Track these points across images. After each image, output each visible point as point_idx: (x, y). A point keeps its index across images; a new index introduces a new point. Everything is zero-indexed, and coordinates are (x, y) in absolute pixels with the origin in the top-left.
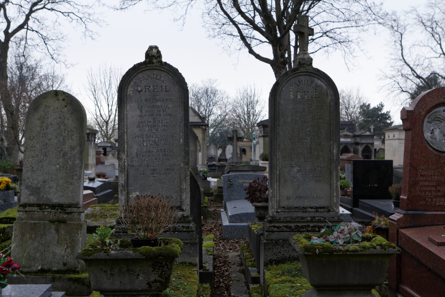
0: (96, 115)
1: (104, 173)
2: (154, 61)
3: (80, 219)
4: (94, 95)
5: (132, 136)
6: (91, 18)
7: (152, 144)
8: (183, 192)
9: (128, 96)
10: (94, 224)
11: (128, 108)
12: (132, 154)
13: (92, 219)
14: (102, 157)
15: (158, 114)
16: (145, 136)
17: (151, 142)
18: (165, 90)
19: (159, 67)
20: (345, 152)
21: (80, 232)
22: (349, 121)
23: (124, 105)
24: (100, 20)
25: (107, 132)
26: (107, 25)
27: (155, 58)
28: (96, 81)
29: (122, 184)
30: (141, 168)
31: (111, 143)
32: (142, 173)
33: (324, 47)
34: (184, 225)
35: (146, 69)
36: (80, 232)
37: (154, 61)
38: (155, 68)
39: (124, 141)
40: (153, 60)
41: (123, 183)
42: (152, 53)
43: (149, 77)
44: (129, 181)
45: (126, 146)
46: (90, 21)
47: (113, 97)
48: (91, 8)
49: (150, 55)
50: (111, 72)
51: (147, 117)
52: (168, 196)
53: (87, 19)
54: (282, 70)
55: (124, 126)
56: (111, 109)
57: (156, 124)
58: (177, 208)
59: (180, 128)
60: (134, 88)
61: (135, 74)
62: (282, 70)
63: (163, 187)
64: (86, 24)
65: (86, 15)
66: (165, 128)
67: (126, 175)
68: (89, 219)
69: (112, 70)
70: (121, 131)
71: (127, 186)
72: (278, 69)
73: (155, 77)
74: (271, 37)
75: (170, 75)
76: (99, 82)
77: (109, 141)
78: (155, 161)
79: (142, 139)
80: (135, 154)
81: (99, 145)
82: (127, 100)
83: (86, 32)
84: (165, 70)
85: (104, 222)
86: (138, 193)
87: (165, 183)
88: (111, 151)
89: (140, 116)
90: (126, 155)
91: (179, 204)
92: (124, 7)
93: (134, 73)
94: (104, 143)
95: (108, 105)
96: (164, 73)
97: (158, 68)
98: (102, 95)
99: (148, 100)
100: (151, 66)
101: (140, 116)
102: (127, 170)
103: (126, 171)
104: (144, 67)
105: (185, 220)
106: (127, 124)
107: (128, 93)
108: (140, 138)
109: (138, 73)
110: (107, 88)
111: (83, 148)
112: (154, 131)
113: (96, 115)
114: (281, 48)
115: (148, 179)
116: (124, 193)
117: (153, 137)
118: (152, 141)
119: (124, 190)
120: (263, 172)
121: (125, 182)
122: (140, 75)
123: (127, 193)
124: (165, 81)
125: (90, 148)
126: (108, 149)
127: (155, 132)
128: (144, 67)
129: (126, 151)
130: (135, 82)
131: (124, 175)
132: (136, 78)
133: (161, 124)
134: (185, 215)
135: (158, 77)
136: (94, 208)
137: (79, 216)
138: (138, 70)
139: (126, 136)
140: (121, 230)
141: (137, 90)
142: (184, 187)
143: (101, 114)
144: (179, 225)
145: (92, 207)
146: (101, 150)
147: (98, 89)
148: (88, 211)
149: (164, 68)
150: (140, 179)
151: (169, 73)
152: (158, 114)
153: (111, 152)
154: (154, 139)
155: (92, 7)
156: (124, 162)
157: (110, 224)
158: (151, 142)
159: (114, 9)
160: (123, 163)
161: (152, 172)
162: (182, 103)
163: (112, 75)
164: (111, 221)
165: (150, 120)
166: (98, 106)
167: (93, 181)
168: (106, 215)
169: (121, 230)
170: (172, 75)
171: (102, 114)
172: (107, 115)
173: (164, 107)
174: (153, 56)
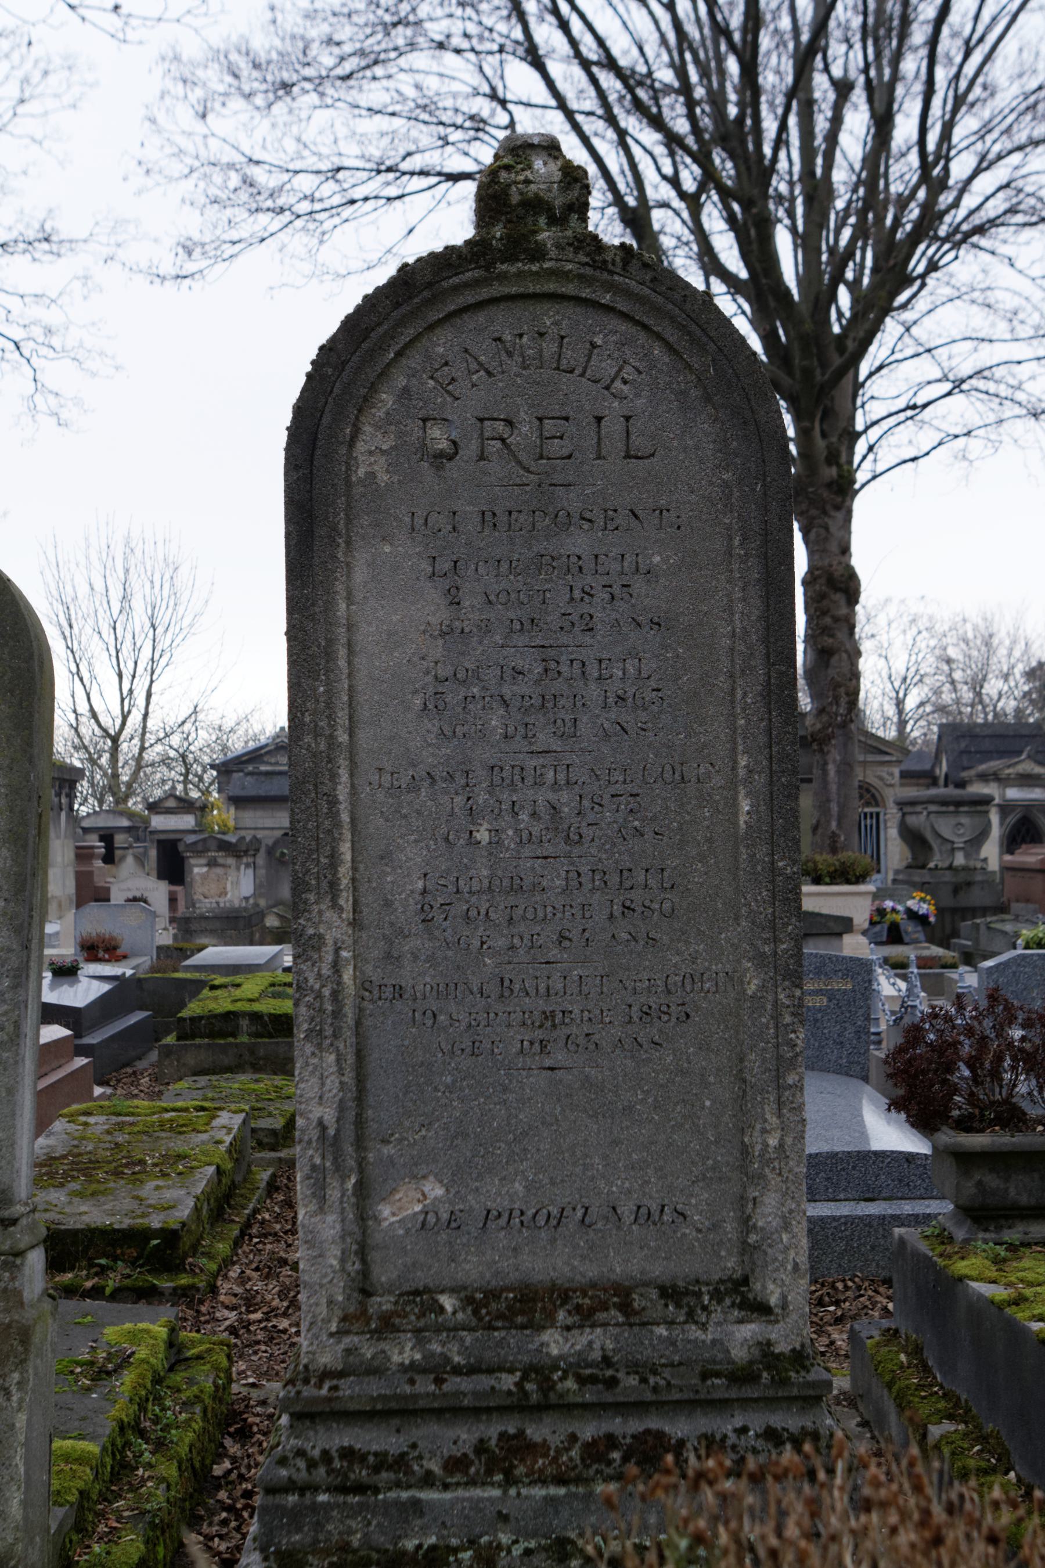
0: (75, 711)
1: (112, 938)
2: (543, 236)
3: (18, 1293)
4: (65, 638)
5: (386, 779)
6: (55, 341)
7: (536, 831)
8: (762, 1176)
9: (358, 490)
10: (86, 1219)
11: (360, 575)
12: (388, 904)
13: (74, 1186)
14: (99, 868)
15: (575, 618)
16: (481, 773)
17: (524, 816)
18: (621, 445)
19: (581, 277)
20: (1024, 841)
21: (16, 1376)
22: (986, 724)
23: (334, 557)
24: (89, 351)
25: (116, 776)
26: (117, 368)
27: (553, 221)
28: (74, 587)
29: (321, 1125)
30: (453, 1008)
31: (131, 815)
32: (467, 1044)
33: (956, 436)
34: (779, 1420)
35: (485, 293)
36: (16, 1376)
37: (543, 236)
38: (551, 287)
39: (333, 813)
40: (535, 232)
41: (329, 1115)
42: (527, 182)
43: (510, 354)
44: (371, 1100)
45: (345, 849)
46: (51, 354)
47: (138, 645)
48: (53, 305)
49: (515, 198)
50: (128, 551)
51: (498, 639)
52: (655, 1208)
53: (39, 348)
54: (833, 513)
55: (329, 705)
56: (131, 691)
57: (558, 686)
58: (717, 1296)
59: (733, 716)
60: (400, 435)
61: (411, 332)
62: (833, 513)
63: (616, 1142)
64: (35, 366)
65: (37, 332)
66: (626, 718)
67: (351, 1059)
68: (62, 1185)
69: (133, 545)
70: (307, 739)
71: (360, 1143)
72: (814, 512)
73: (546, 354)
74: (790, 381)
75: (659, 337)
76: (83, 590)
77: (122, 806)
78: (554, 953)
79: (459, 800)
80: (413, 907)
81: (85, 824)
82: (349, 521)
83: (38, 398)
84: (623, 306)
85: (135, 1205)
86: (439, 1192)
87: (629, 1109)
88: (130, 847)
89: (443, 634)
90: (348, 915)
91: (731, 1264)
92: (190, 267)
93: (401, 323)
94: (103, 815)
95: (120, 675)
96: (615, 323)
97: (570, 289)
98: (96, 636)
99: (502, 518)
100: (520, 274)
101: (443, 634)
102: (358, 1023)
103: (348, 1033)
104: (476, 283)
105: (785, 1382)
106: (351, 687)
107: (361, 472)
108: (445, 791)
109: (431, 328)
110: (115, 611)
111: (35, 857)
112: (544, 739)
113: (75, 711)
114: (825, 427)
115: (505, 1089)
116: (337, 1194)
117: (538, 784)
118: (534, 815)
119: (338, 1167)
120: (834, 941)
121: (341, 1108)
122: (442, 343)
123: (360, 1185)
124: (618, 384)
125: (52, 834)
126: (120, 839)
127: (556, 745)
128: (476, 283)
129: (345, 882)
130: (406, 390)
131: (332, 1058)
132: (414, 360)
133: (593, 692)
134: (782, 1347)
135: (572, 356)
136: (83, 1119)
137: (13, 1279)
138: (430, 302)
139: (344, 777)
140: (322, 1470)
141: (423, 450)
142: (773, 1142)
143: (92, 710)
144: (738, 1422)
145: (72, 1118)
146: (94, 841)
147: (80, 615)
148: (51, 1141)
149: (610, 287)
150: (450, 1088)
151: (650, 322)
152: (575, 618)
153: (131, 851)
154: (551, 796)
155: (59, 302)
156: (336, 967)
157: (162, 1216)
158: (524, 816)
159: (149, 278)
160: (326, 971)
161: (539, 1034)
162: (745, 538)
163: (132, 562)
164: (169, 1195)
165: (519, 663)
166: (81, 680)
167: (71, 979)
168: (142, 1162)
169: (322, 1470)
170: (672, 335)
171: (96, 709)
172: (117, 711)
173: (615, 567)
174: (535, 205)
